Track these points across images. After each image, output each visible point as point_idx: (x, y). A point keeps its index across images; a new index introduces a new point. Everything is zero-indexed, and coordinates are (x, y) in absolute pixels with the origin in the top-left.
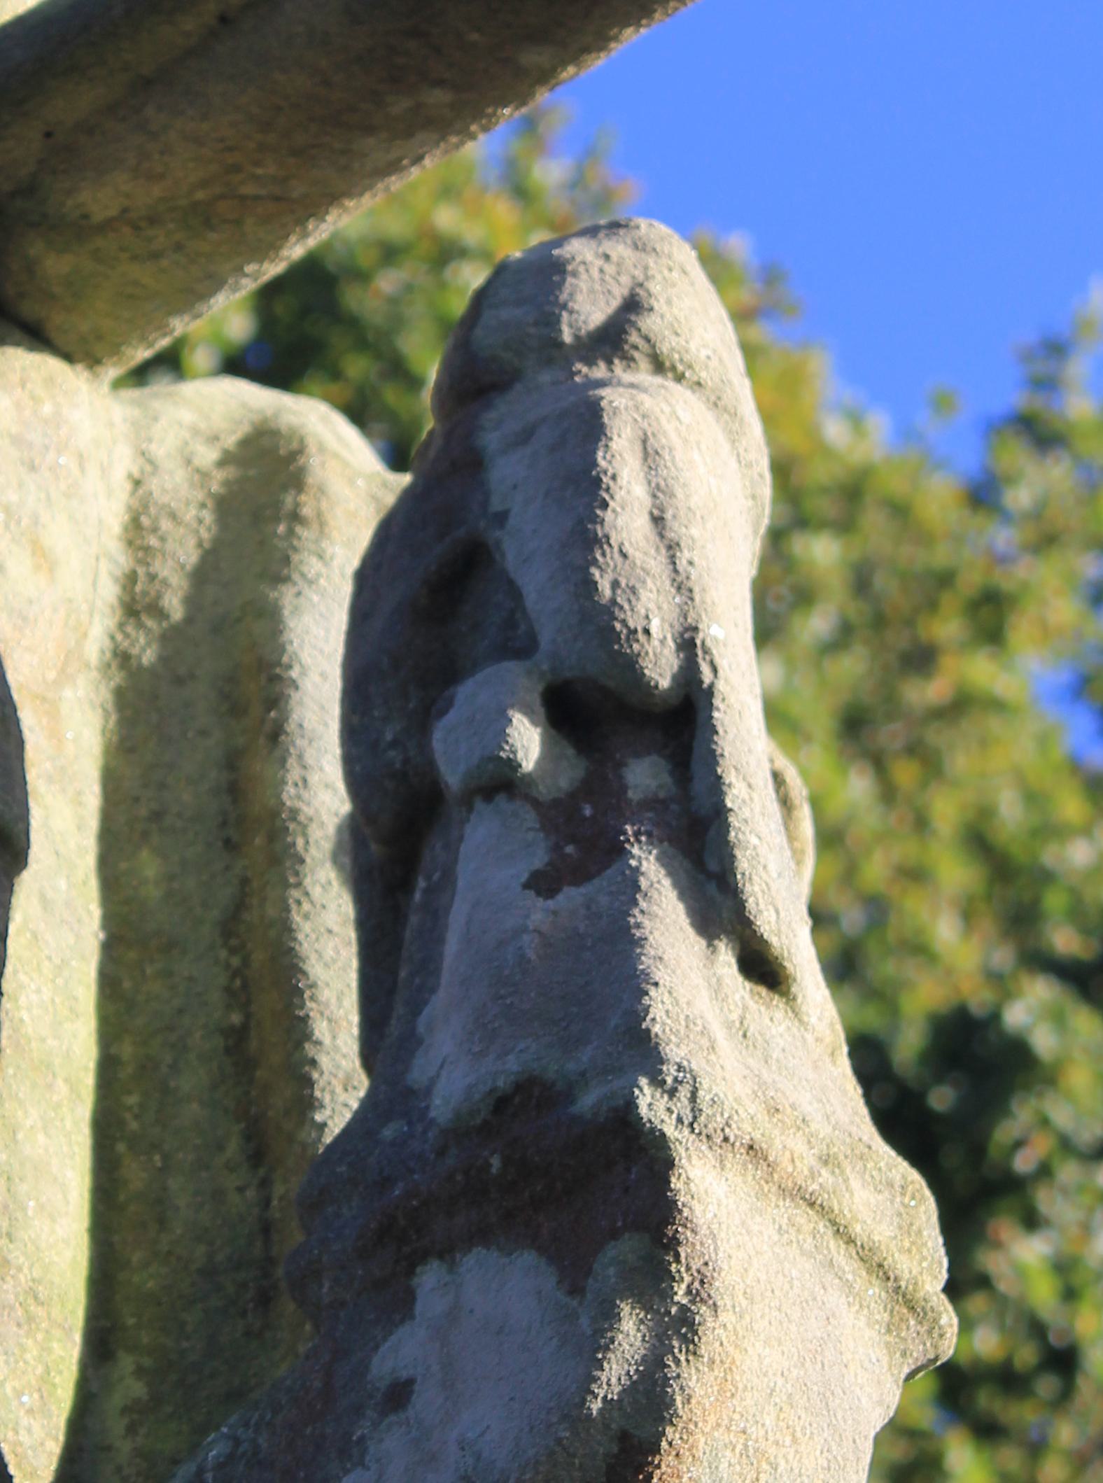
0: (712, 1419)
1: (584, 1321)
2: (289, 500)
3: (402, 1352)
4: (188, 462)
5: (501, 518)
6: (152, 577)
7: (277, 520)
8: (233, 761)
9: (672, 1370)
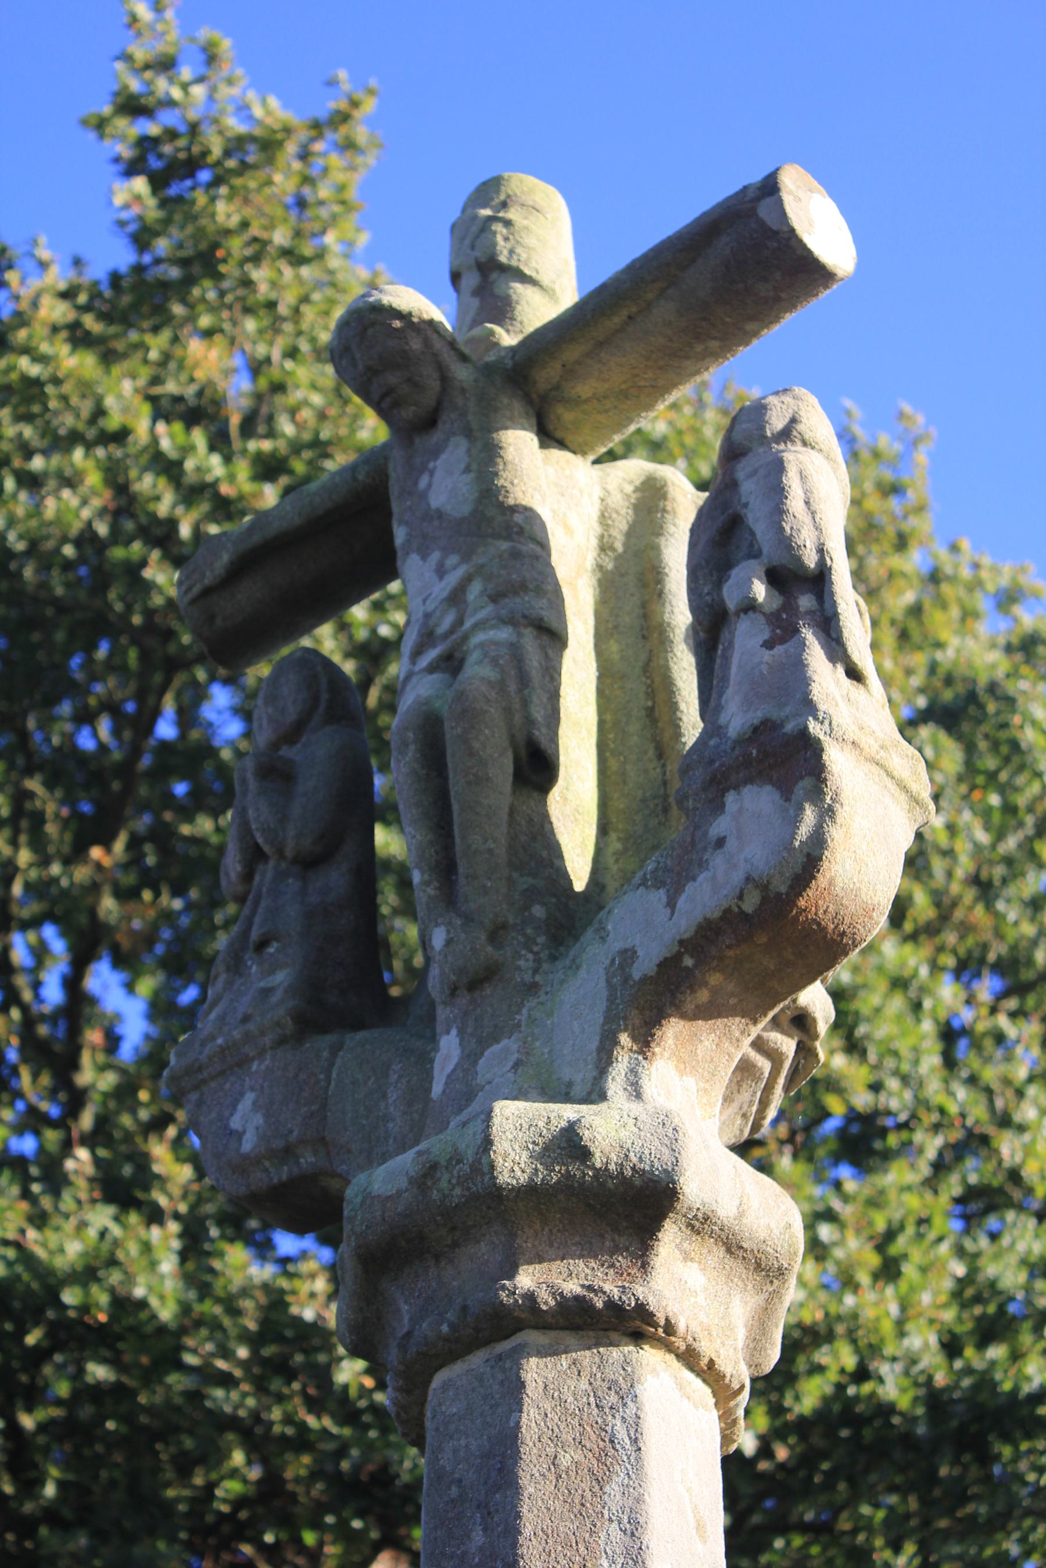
0: (842, 848)
1: (791, 812)
2: (661, 504)
3: (721, 826)
4: (622, 491)
5: (746, 505)
6: (610, 536)
7: (657, 512)
8: (644, 605)
9: (826, 829)
